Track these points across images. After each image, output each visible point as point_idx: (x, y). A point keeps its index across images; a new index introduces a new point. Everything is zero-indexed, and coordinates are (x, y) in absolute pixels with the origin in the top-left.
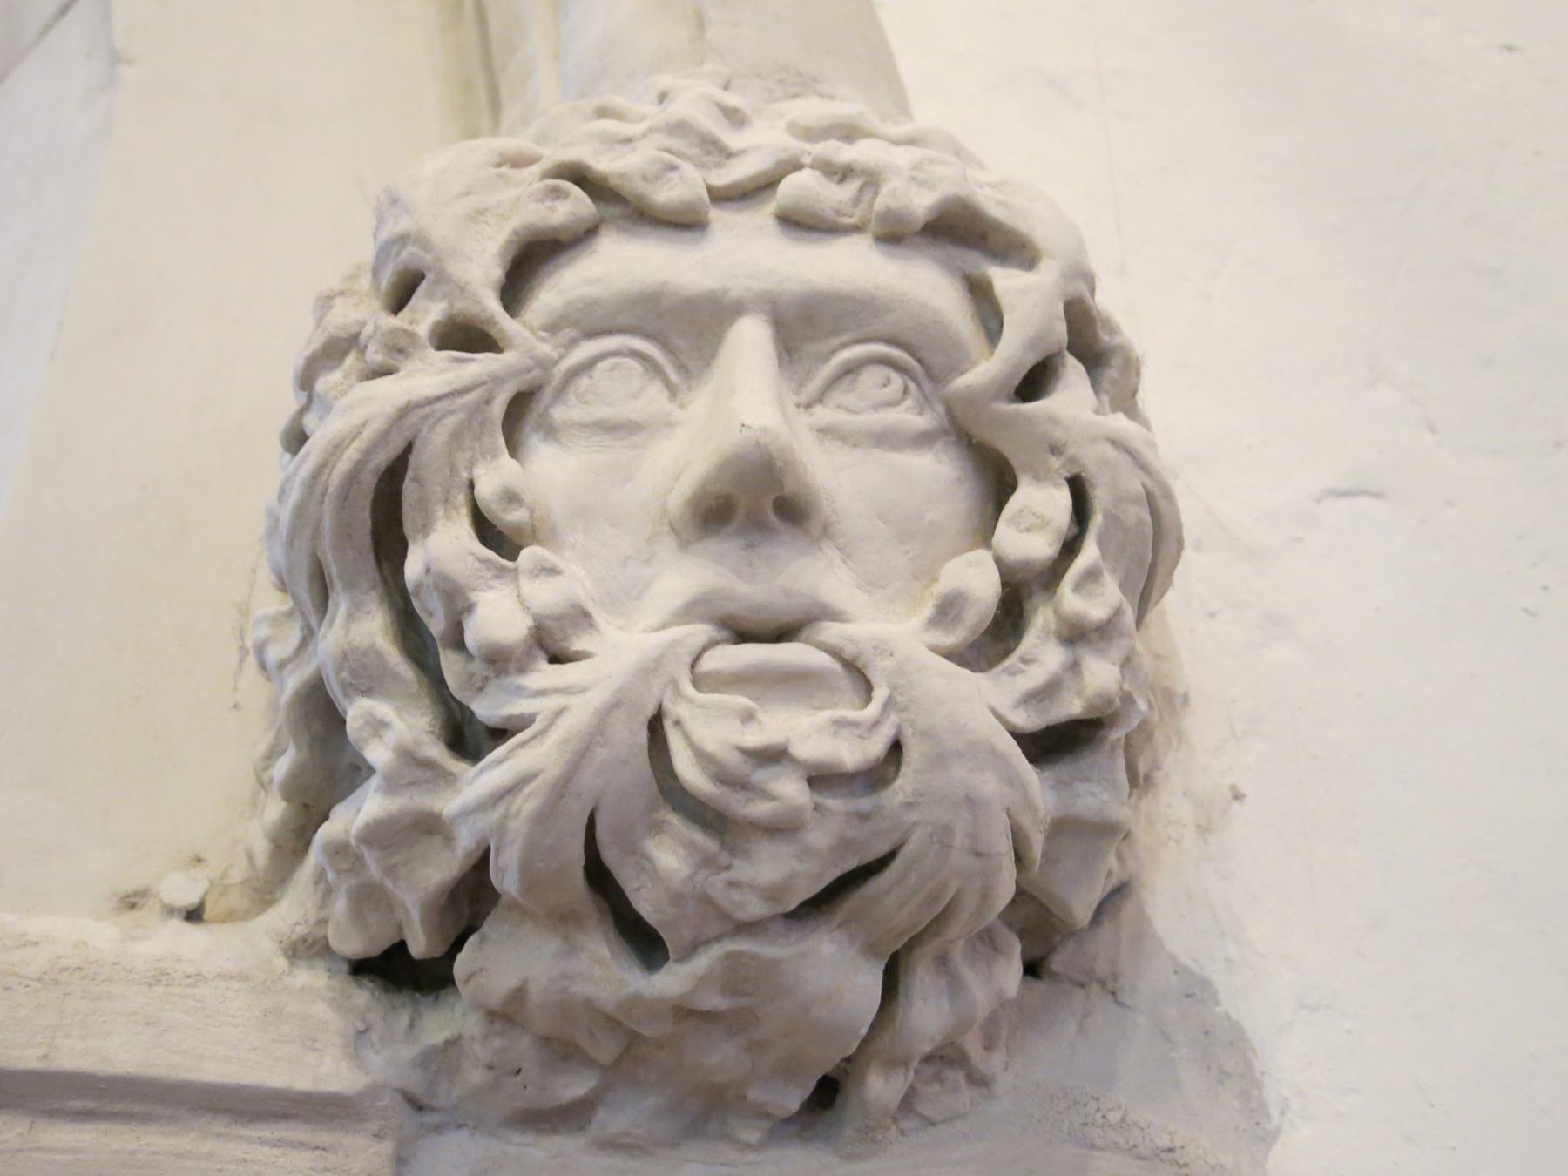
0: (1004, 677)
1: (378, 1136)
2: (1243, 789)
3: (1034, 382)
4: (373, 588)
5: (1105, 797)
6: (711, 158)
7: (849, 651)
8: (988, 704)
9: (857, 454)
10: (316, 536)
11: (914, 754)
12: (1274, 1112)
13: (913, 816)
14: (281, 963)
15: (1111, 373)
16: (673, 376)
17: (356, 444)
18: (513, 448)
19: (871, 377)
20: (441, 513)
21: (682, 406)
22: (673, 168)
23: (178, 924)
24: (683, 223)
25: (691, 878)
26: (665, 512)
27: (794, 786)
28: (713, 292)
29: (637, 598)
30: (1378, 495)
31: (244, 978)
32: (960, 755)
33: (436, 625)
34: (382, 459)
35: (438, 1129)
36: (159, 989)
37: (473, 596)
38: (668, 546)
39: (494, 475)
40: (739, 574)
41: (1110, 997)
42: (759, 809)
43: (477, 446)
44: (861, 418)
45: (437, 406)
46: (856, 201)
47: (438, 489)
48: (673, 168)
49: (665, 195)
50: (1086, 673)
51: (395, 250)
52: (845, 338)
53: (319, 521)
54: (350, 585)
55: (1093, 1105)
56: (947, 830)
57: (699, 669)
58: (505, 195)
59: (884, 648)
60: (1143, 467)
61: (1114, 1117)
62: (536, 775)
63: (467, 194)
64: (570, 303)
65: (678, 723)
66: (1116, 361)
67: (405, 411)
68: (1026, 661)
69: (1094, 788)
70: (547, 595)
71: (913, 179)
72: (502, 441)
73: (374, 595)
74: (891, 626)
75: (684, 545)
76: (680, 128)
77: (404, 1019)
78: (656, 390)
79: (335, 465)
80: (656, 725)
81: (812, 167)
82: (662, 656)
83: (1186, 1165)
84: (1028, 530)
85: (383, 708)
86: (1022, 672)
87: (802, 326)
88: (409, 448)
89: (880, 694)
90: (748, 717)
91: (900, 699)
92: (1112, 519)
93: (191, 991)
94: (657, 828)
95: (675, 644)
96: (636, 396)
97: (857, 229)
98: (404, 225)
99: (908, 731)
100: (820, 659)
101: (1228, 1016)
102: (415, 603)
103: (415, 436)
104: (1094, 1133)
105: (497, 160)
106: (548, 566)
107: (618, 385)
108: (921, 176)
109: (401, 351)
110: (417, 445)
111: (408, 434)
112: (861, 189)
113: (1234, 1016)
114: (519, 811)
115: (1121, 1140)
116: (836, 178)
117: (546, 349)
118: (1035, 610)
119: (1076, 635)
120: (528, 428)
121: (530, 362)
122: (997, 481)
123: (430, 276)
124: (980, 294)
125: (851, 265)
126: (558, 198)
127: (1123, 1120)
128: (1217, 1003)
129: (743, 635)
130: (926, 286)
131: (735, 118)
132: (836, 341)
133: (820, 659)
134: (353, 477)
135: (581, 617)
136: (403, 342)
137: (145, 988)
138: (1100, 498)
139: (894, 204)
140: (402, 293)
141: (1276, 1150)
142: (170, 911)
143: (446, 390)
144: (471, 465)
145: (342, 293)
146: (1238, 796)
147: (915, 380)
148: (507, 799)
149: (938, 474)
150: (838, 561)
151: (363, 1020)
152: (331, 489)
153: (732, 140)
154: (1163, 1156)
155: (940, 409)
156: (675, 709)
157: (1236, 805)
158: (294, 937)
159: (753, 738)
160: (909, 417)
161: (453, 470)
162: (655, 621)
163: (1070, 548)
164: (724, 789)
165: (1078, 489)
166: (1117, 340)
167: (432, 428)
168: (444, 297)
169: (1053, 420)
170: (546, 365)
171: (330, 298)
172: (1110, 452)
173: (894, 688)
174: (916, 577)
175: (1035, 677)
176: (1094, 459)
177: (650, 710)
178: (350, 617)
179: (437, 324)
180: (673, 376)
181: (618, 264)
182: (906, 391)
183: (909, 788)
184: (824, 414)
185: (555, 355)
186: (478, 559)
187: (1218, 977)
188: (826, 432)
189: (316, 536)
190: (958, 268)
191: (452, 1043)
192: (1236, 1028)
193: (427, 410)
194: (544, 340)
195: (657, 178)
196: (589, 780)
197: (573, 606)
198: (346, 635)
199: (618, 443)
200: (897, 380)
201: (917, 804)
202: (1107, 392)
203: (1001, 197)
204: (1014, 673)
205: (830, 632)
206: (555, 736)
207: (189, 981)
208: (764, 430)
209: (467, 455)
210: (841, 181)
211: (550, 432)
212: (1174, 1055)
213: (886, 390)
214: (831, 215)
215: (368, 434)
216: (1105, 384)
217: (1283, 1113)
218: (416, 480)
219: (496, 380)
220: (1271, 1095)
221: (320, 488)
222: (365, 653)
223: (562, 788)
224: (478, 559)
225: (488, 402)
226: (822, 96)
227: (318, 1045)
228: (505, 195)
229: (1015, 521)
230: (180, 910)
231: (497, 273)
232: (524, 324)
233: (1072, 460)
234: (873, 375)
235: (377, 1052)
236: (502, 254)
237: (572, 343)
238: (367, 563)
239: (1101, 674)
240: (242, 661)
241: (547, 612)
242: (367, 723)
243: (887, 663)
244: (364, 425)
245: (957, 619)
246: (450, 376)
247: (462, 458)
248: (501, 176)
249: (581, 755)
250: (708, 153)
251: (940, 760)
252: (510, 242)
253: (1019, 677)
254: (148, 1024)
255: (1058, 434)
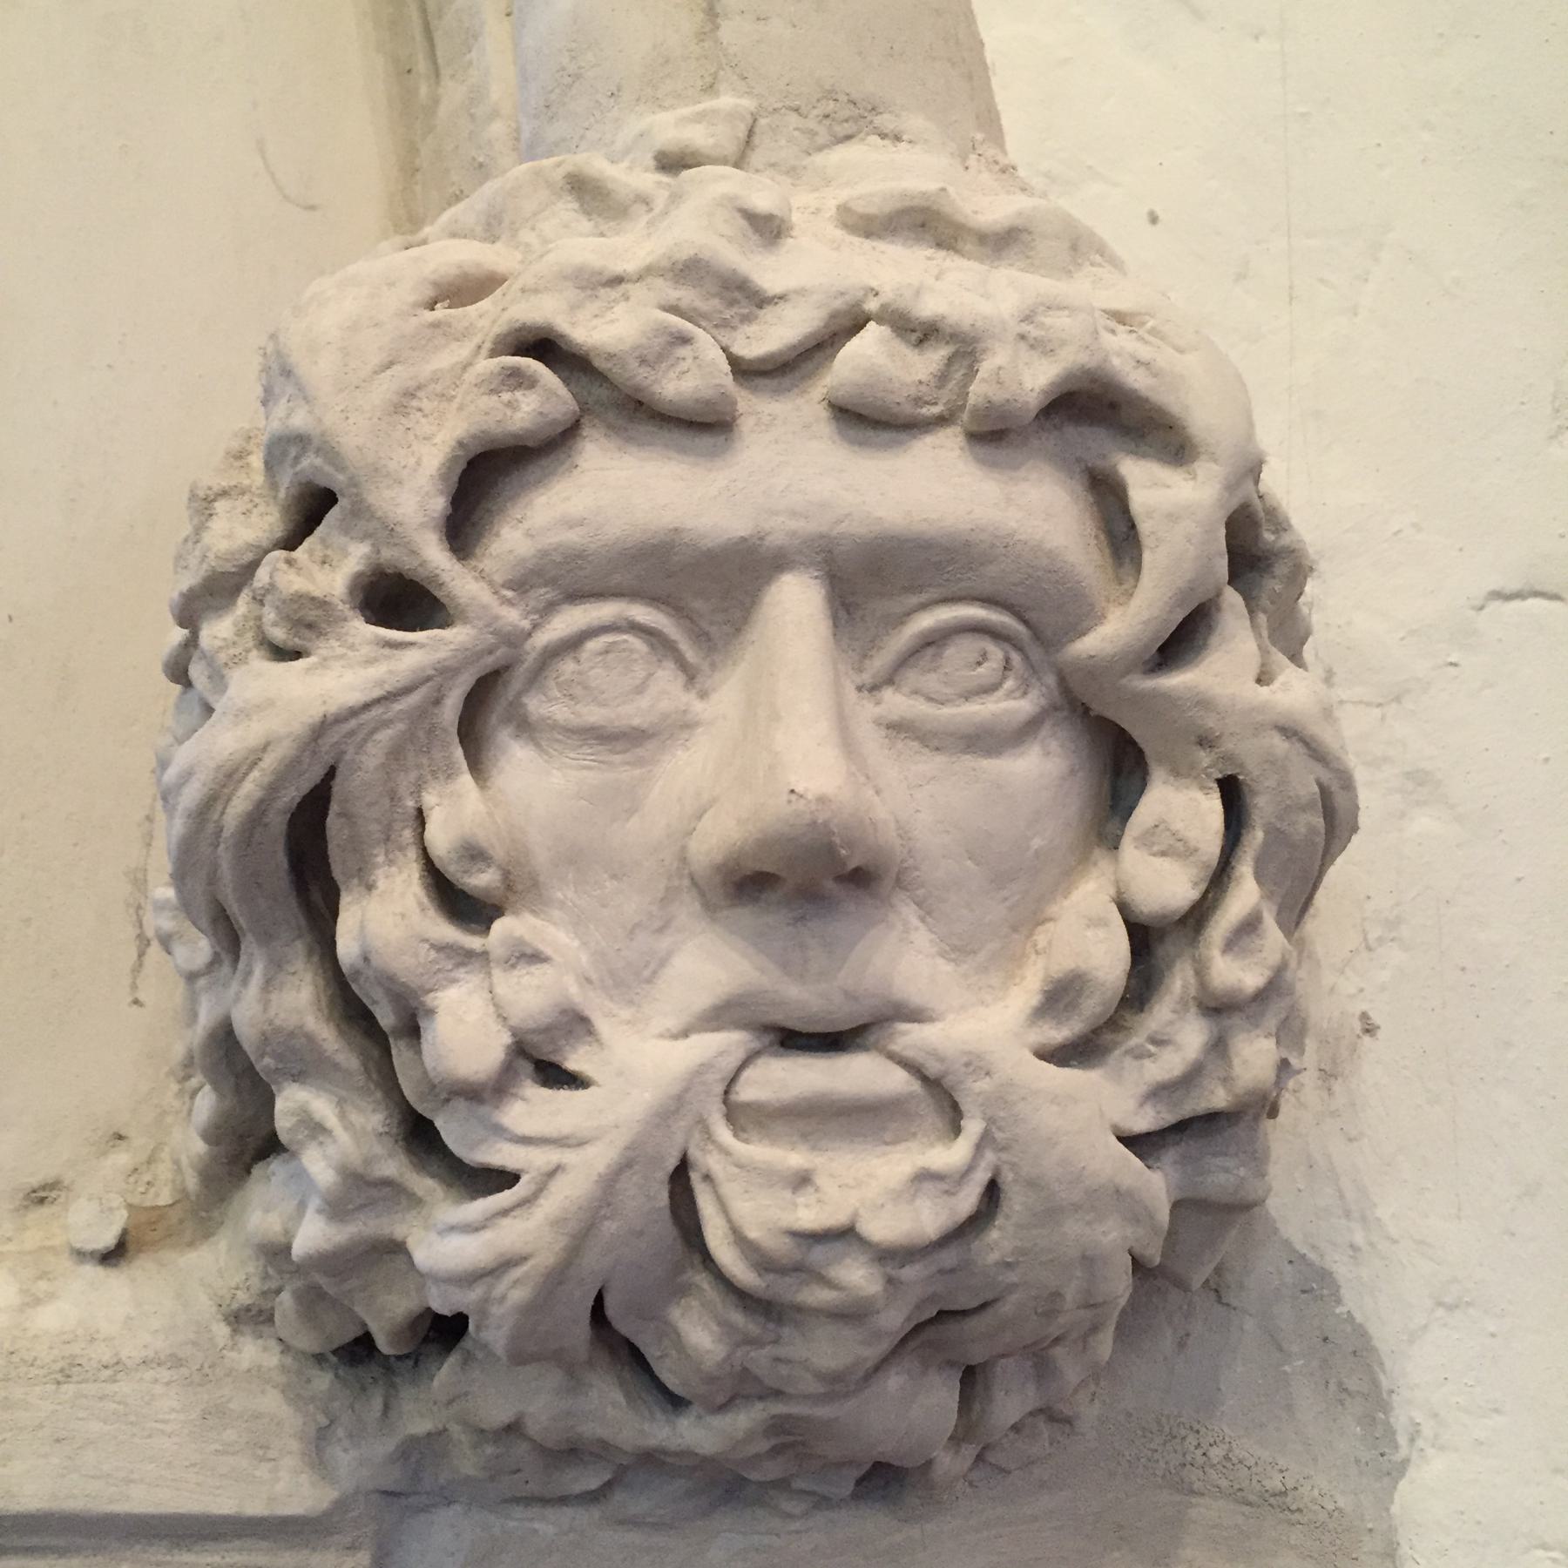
0: (1128, 1062)
1: (352, 1548)
2: (1376, 1018)
3: (1182, 639)
4: (299, 937)
5: (1242, 1172)
6: (735, 310)
7: (933, 1068)
8: (1112, 1097)
9: (940, 760)
10: (213, 880)
11: (1015, 1201)
12: (1402, 1440)
13: (1012, 1277)
14: (222, 1331)
15: (1273, 585)
16: (690, 654)
17: (255, 774)
18: (477, 764)
19: (960, 652)
20: (381, 859)
21: (703, 695)
22: (684, 340)
23: (92, 1271)
24: (705, 426)
25: (729, 1357)
26: (683, 860)
27: (861, 1272)
28: (744, 539)
29: (649, 981)
30: (1555, 597)
31: (176, 1362)
32: (1077, 1207)
33: (386, 1018)
34: (292, 795)
35: (425, 1509)
36: (69, 1389)
37: (429, 1000)
38: (687, 910)
39: (456, 811)
40: (785, 966)
41: (1213, 1295)
42: (818, 1296)
43: (425, 761)
44: (947, 711)
45: (365, 717)
46: (942, 378)
47: (374, 827)
48: (684, 340)
49: (678, 384)
50: (1236, 1062)
51: (293, 452)
52: (924, 597)
53: (215, 867)
54: (266, 938)
55: (1192, 1440)
56: (1057, 1295)
57: (733, 1097)
58: (446, 358)
59: (977, 1064)
60: (1316, 753)
61: (1216, 1453)
62: (524, 1259)
63: (390, 365)
64: (544, 553)
65: (707, 1178)
66: (1281, 569)
67: (322, 728)
68: (1158, 1042)
69: (1230, 1163)
70: (530, 995)
71: (1022, 337)
72: (459, 752)
73: (300, 947)
74: (984, 1021)
75: (710, 908)
76: (690, 270)
77: (377, 1403)
78: (667, 678)
79: (229, 800)
80: (681, 1175)
81: (880, 320)
82: (686, 1090)
83: (1299, 1510)
84: (1163, 854)
85: (322, 1106)
86: (1150, 1055)
87: (869, 580)
88: (331, 773)
89: (973, 1127)
90: (802, 1180)
91: (999, 1135)
92: (1276, 835)
93: (111, 1388)
94: (683, 1291)
95: (703, 1069)
96: (640, 689)
97: (942, 421)
98: (300, 420)
99: (1007, 1177)
100: (895, 1081)
101: (1350, 1317)
102: (354, 987)
103: (338, 761)
104: (1193, 1475)
105: (430, 293)
106: (529, 951)
107: (618, 679)
108: (1033, 331)
109: (310, 626)
110: (342, 771)
111: (328, 759)
112: (950, 361)
113: (1359, 1318)
114: (503, 1298)
115: (1224, 1483)
116: (914, 337)
117: (513, 617)
118: (1170, 967)
119: (1219, 1008)
120: (494, 719)
121: (491, 639)
122: (1118, 765)
123: (343, 502)
124: (1107, 496)
125: (931, 488)
126: (519, 386)
127: (1226, 1458)
128: (1339, 1302)
129: (793, 1039)
130: (1033, 509)
131: (768, 229)
132: (914, 600)
133: (895, 1081)
134: (256, 818)
135: (576, 1024)
136: (312, 615)
137: (51, 1387)
138: (1262, 807)
139: (998, 396)
140: (312, 509)
141: (1403, 1485)
142: (81, 1255)
143: (377, 693)
144: (418, 788)
145: (224, 493)
146: (1370, 1030)
147: (1019, 648)
148: (488, 1279)
149: (1043, 770)
150: (915, 921)
151: (326, 1412)
152: (226, 834)
153: (768, 272)
154: (1272, 1500)
155: (1051, 680)
156: (710, 1161)
157: (1367, 1039)
158: (235, 1306)
159: (809, 1214)
160: (1011, 705)
161: (394, 797)
162: (673, 1023)
163: (1220, 878)
164: (771, 1277)
165: (1232, 792)
166: (1286, 540)
167: (360, 747)
168: (365, 536)
169: (1204, 703)
170: (513, 640)
171: (209, 501)
172: (1279, 744)
173: (991, 1121)
174: (1015, 929)
175: (1169, 1065)
176: (1254, 754)
177: (672, 1163)
178: (268, 985)
179: (358, 576)
180: (690, 654)
181: (611, 491)
182: (1007, 666)
183: (1007, 1245)
184: (896, 703)
185: (526, 624)
186: (433, 946)
187: (1341, 1268)
188: (898, 728)
189: (213, 880)
190: (1079, 460)
191: (438, 1435)
192: (1361, 1332)
193: (353, 723)
194: (510, 603)
195: (661, 357)
196: (593, 1262)
197: (564, 1012)
198: (265, 1010)
199: (617, 758)
200: (996, 653)
201: (1018, 1263)
202: (1265, 612)
203: (1145, 352)
204: (1139, 1055)
205: (910, 1037)
206: (549, 1206)
207: (108, 1373)
208: (822, 800)
209: (413, 776)
210: (921, 342)
211: (525, 727)
212: (1287, 1368)
213: (980, 670)
214: (908, 409)
215: (270, 762)
216: (1265, 601)
217: (1412, 1440)
218: (342, 814)
219: (445, 672)
220: (1400, 1420)
221: (210, 828)
222: (292, 1035)
223: (557, 1277)
224: (433, 946)
225: (437, 702)
226: (883, 136)
227: (271, 1454)
228: (446, 358)
229: (1147, 840)
230: (92, 1253)
231: (439, 504)
232: (482, 576)
233: (1227, 758)
234: (967, 647)
235: (345, 1450)
236: (444, 477)
237: (549, 609)
238: (290, 910)
239: (1255, 1056)
240: (141, 955)
241: (531, 1024)
242: (302, 1122)
243: (983, 1085)
244: (265, 748)
245: (1072, 1006)
246: (378, 671)
247: (404, 782)
248: (436, 325)
249: (581, 1233)
250: (732, 303)
251: (1052, 1213)
252: (454, 459)
253: (1147, 1062)
254: (58, 1441)
255: (1211, 722)
